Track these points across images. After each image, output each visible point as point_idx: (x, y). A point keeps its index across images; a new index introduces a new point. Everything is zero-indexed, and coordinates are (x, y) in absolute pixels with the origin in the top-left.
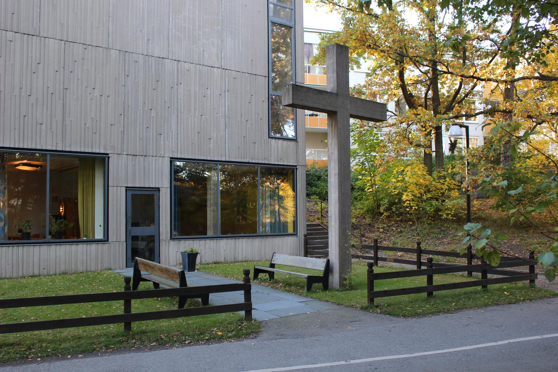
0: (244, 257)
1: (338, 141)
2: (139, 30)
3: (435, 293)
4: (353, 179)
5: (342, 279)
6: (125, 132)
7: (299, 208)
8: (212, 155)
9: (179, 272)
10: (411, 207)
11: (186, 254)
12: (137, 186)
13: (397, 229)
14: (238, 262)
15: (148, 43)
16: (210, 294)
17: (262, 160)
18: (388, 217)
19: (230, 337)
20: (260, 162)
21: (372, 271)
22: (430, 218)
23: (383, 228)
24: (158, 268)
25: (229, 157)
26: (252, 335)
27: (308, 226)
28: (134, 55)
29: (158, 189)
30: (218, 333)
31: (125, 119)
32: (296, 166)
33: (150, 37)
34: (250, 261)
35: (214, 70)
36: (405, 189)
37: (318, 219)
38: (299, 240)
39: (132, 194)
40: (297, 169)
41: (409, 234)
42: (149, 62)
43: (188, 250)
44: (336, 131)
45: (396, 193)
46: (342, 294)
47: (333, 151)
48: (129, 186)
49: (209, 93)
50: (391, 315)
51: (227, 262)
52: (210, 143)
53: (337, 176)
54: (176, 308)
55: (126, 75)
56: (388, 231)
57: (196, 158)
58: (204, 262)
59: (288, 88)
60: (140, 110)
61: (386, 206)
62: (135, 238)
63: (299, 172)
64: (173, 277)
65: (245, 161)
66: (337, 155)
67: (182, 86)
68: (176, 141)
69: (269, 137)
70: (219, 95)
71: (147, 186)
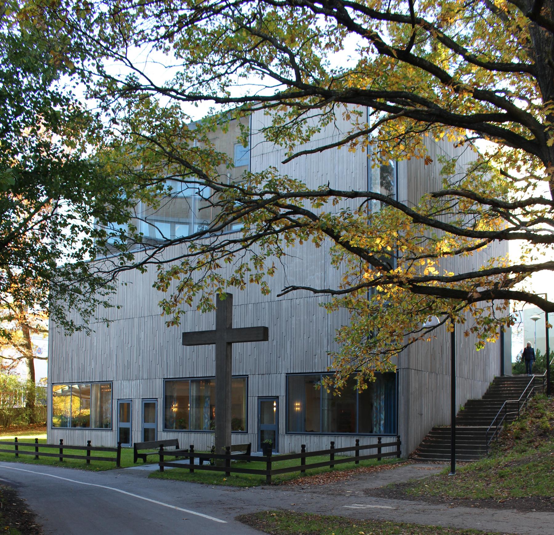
3: (195, 471)
49: (314, 318)
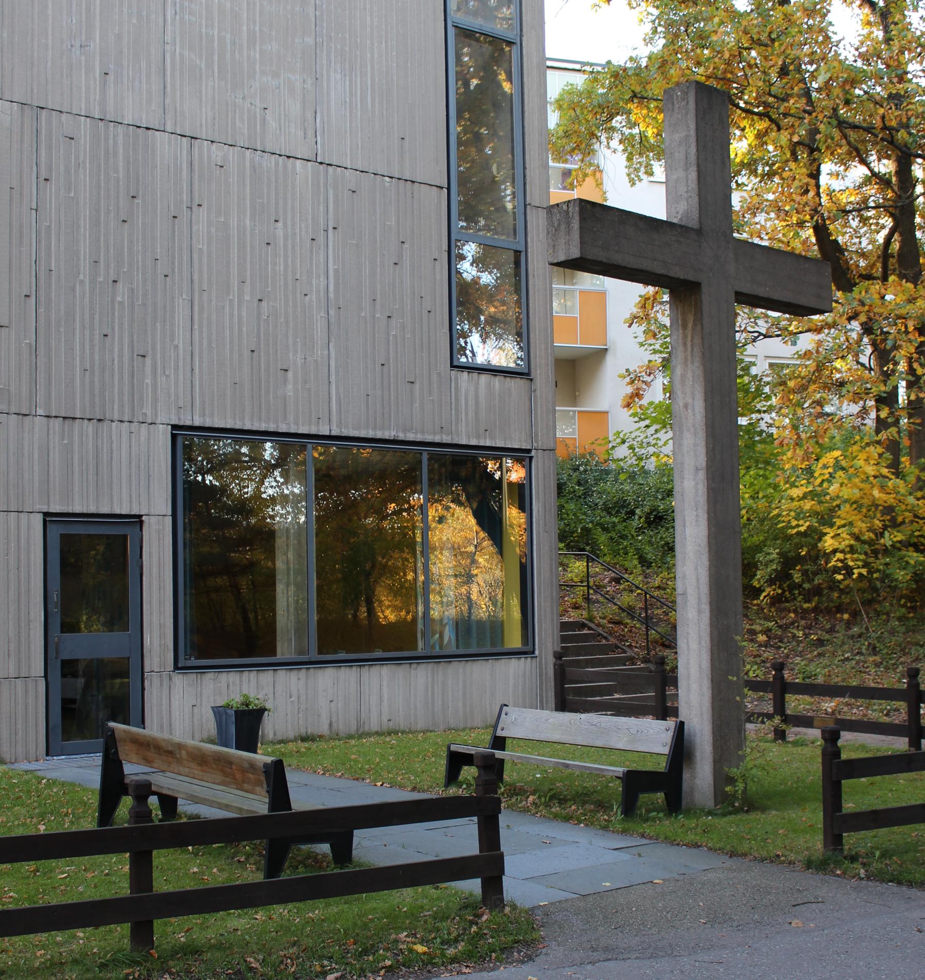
0: (385, 720)
1: (705, 372)
2: (78, 44)
4: (657, 491)
5: (722, 779)
6: (41, 351)
7: (539, 574)
8: (291, 418)
9: (266, 765)
10: (849, 571)
11: (231, 712)
12: (78, 509)
13: (806, 635)
14: (369, 734)
15: (104, 84)
16: (356, 832)
17: (434, 433)
18: (776, 601)
19: (454, 960)
20: (429, 438)
21: (837, 753)
22: (903, 602)
23: (767, 632)
24: (187, 752)
25: (340, 425)
26: (519, 952)
27: (564, 626)
28: (64, 116)
29: (137, 521)
30: (415, 947)
31: (41, 310)
32: (529, 451)
33: (111, 66)
34: (403, 732)
35: (294, 167)
36: (827, 518)
37: (576, 607)
38: (541, 668)
39: (62, 536)
40: (531, 458)
41: (846, 647)
42: (106, 140)
43: (236, 699)
44: (698, 340)
45: (802, 529)
46: (730, 824)
47: (690, 401)
48: (51, 510)
49: (280, 233)
50: (900, 883)
51: (336, 737)
52: (285, 381)
53: (702, 475)
54: (252, 875)
55: (41, 179)
56: (781, 641)
57: (246, 428)
58: (271, 736)
59: (567, 212)
60: (82, 282)
61: (774, 567)
62: (69, 668)
63: (537, 468)
64: (244, 781)
65: (387, 435)
66: (702, 410)
67: (203, 212)
68: (189, 374)
69: (452, 366)
70: (309, 241)
71: (105, 510)
